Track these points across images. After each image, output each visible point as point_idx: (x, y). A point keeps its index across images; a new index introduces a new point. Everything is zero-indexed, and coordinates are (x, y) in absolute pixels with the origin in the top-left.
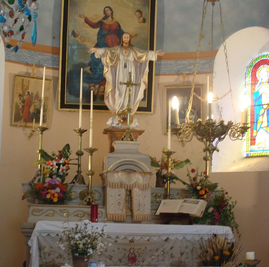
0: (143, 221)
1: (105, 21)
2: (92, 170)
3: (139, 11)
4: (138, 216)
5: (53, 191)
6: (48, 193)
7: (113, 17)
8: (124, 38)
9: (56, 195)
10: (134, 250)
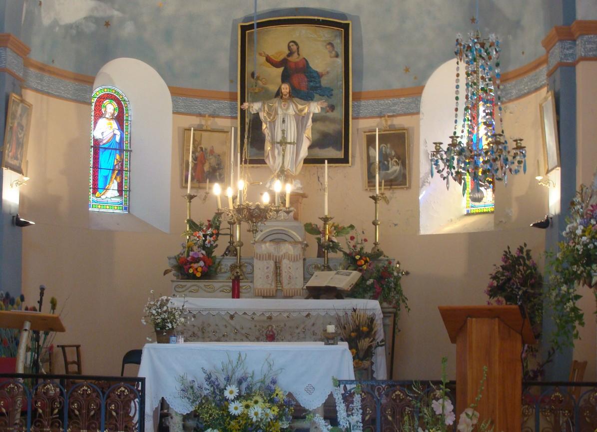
0: (295, 295)
1: (290, 59)
2: (241, 240)
3: (331, 44)
4: (288, 291)
5: (195, 265)
6: (191, 267)
7: (300, 53)
8: (282, 89)
9: (200, 269)
10: (272, 327)
